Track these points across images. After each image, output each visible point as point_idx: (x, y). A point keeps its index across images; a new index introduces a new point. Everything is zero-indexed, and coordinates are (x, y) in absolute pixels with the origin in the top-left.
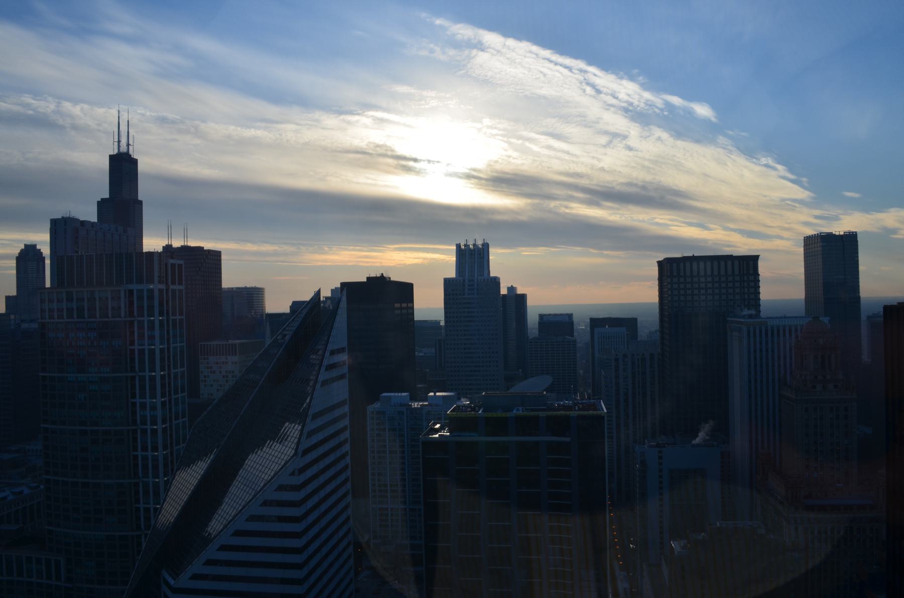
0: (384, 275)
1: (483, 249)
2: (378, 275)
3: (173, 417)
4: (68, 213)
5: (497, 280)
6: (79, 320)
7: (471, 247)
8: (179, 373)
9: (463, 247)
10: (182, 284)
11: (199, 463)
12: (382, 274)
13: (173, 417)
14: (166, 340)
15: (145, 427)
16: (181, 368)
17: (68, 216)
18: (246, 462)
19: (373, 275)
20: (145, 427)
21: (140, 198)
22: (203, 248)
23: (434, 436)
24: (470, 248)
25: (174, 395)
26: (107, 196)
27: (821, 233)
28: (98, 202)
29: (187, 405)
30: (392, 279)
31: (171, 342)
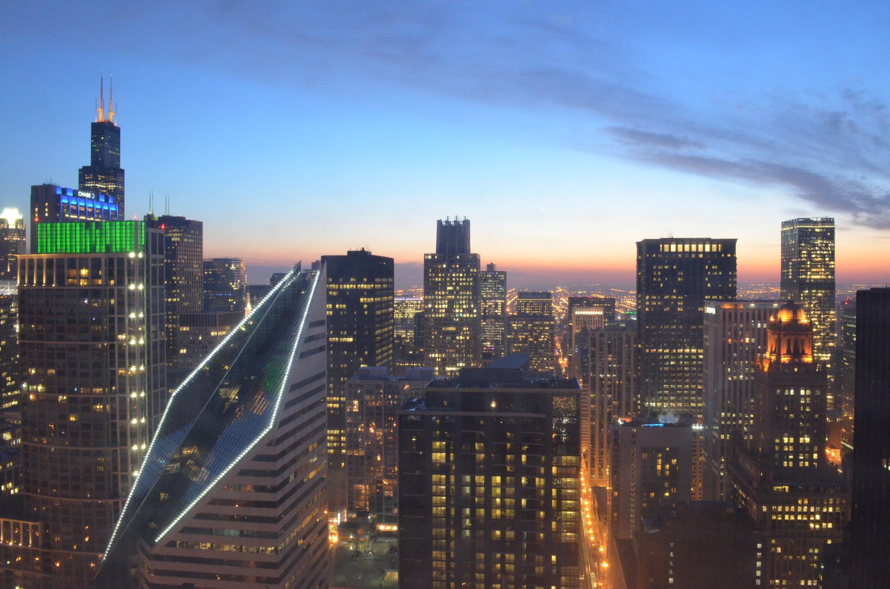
0: (365, 250)
1: (464, 226)
2: (359, 250)
3: (153, 412)
4: (49, 180)
5: (478, 258)
6: (111, 477)
7: (452, 223)
8: (158, 342)
9: (444, 223)
10: (163, 254)
11: (178, 431)
12: (363, 248)
13: (153, 412)
14: (146, 379)
15: (113, 316)
16: (161, 387)
17: (49, 183)
18: (224, 432)
19: (354, 249)
20: (113, 316)
21: (122, 167)
22: (185, 218)
23: (411, 410)
24: (451, 225)
25: (154, 389)
26: (88, 163)
27: (798, 219)
28: (80, 170)
29: (166, 374)
30: (373, 254)
31: (151, 312)
